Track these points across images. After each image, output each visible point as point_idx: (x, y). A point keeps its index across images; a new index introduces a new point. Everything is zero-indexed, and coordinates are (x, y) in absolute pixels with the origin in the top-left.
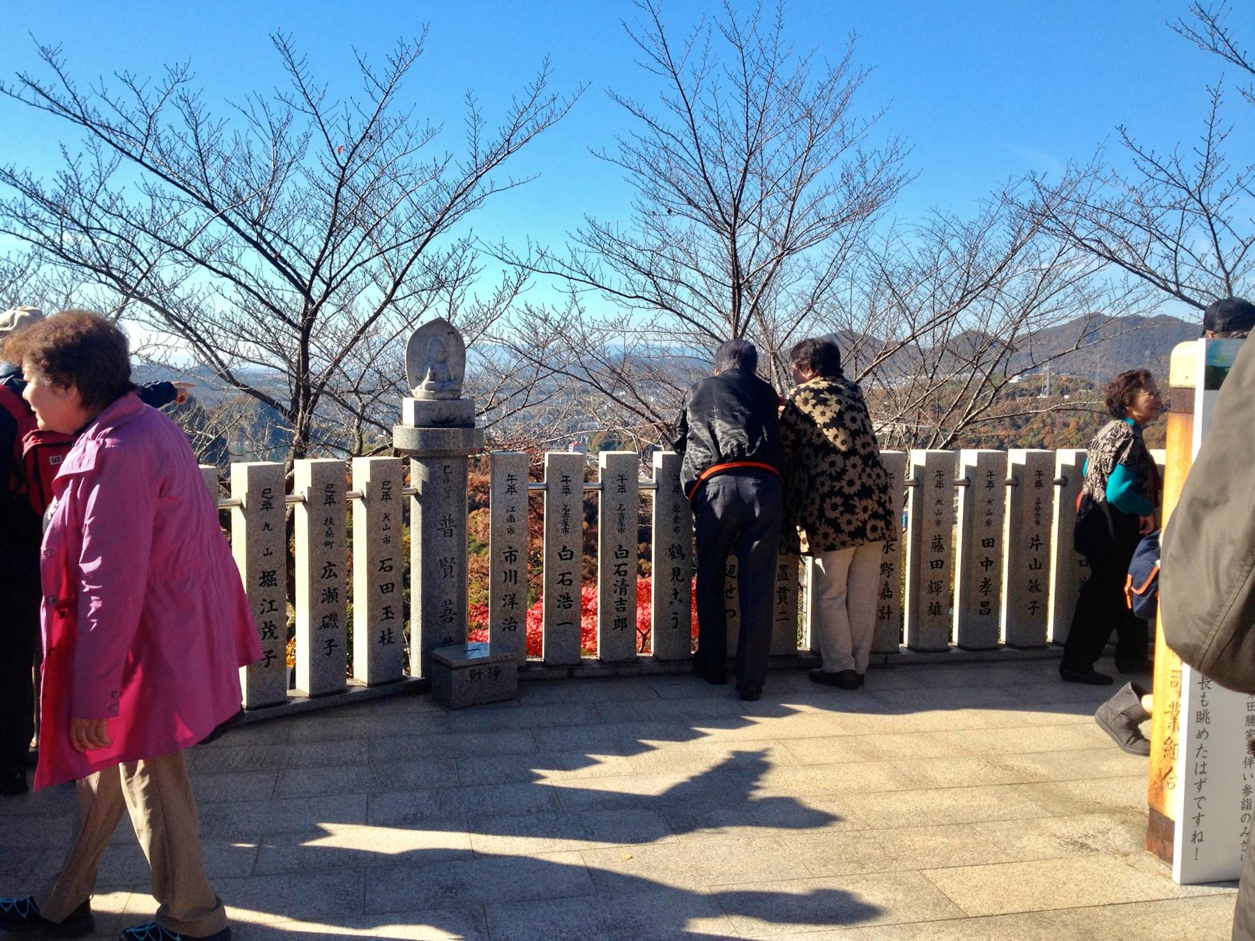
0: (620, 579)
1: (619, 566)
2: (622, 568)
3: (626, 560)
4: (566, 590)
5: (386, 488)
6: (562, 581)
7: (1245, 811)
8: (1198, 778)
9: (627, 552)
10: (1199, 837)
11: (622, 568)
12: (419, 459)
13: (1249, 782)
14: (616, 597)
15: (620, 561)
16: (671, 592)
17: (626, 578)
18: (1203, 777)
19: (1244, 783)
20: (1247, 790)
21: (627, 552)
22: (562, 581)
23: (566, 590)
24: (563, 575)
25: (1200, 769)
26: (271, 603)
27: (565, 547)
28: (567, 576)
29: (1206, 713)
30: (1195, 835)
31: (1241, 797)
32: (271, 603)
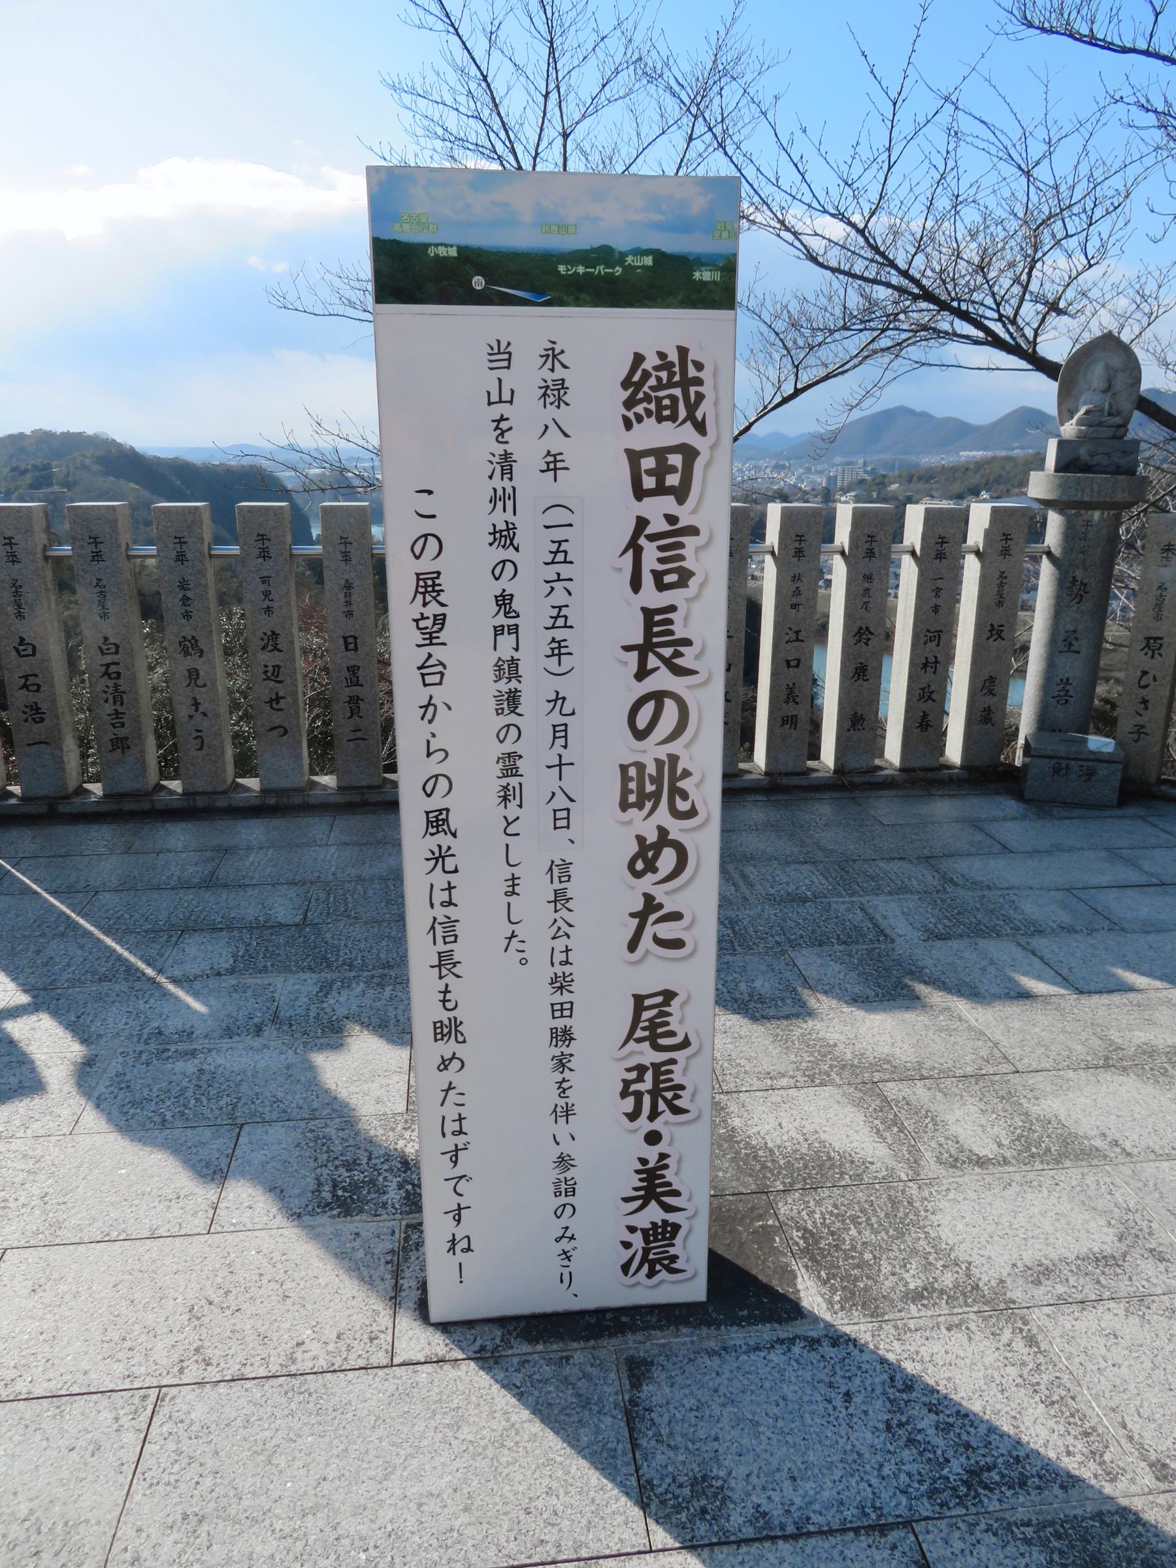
0: (111, 683)
1: (108, 666)
2: (113, 669)
3: (116, 658)
4: (32, 698)
5: (1014, 535)
6: (25, 686)
7: (563, 1200)
8: (450, 1143)
9: (117, 646)
10: (464, 1244)
11: (113, 669)
12: (1061, 512)
13: (567, 1147)
14: (109, 708)
15: (108, 659)
16: (190, 702)
17: (121, 682)
18: (461, 1140)
19: (556, 1152)
20: (564, 1162)
21: (117, 646)
22: (25, 686)
23: (32, 698)
24: (26, 677)
25: (451, 1127)
26: (797, 632)
27: (22, 639)
28: (31, 680)
29: (456, 1024)
30: (453, 1242)
31: (554, 1174)
32: (797, 632)
